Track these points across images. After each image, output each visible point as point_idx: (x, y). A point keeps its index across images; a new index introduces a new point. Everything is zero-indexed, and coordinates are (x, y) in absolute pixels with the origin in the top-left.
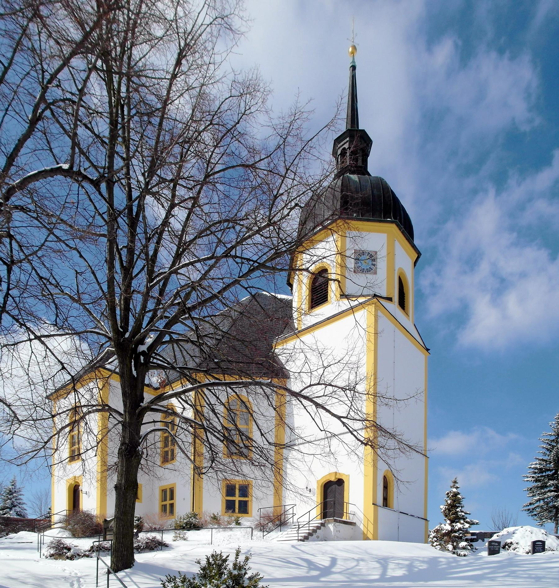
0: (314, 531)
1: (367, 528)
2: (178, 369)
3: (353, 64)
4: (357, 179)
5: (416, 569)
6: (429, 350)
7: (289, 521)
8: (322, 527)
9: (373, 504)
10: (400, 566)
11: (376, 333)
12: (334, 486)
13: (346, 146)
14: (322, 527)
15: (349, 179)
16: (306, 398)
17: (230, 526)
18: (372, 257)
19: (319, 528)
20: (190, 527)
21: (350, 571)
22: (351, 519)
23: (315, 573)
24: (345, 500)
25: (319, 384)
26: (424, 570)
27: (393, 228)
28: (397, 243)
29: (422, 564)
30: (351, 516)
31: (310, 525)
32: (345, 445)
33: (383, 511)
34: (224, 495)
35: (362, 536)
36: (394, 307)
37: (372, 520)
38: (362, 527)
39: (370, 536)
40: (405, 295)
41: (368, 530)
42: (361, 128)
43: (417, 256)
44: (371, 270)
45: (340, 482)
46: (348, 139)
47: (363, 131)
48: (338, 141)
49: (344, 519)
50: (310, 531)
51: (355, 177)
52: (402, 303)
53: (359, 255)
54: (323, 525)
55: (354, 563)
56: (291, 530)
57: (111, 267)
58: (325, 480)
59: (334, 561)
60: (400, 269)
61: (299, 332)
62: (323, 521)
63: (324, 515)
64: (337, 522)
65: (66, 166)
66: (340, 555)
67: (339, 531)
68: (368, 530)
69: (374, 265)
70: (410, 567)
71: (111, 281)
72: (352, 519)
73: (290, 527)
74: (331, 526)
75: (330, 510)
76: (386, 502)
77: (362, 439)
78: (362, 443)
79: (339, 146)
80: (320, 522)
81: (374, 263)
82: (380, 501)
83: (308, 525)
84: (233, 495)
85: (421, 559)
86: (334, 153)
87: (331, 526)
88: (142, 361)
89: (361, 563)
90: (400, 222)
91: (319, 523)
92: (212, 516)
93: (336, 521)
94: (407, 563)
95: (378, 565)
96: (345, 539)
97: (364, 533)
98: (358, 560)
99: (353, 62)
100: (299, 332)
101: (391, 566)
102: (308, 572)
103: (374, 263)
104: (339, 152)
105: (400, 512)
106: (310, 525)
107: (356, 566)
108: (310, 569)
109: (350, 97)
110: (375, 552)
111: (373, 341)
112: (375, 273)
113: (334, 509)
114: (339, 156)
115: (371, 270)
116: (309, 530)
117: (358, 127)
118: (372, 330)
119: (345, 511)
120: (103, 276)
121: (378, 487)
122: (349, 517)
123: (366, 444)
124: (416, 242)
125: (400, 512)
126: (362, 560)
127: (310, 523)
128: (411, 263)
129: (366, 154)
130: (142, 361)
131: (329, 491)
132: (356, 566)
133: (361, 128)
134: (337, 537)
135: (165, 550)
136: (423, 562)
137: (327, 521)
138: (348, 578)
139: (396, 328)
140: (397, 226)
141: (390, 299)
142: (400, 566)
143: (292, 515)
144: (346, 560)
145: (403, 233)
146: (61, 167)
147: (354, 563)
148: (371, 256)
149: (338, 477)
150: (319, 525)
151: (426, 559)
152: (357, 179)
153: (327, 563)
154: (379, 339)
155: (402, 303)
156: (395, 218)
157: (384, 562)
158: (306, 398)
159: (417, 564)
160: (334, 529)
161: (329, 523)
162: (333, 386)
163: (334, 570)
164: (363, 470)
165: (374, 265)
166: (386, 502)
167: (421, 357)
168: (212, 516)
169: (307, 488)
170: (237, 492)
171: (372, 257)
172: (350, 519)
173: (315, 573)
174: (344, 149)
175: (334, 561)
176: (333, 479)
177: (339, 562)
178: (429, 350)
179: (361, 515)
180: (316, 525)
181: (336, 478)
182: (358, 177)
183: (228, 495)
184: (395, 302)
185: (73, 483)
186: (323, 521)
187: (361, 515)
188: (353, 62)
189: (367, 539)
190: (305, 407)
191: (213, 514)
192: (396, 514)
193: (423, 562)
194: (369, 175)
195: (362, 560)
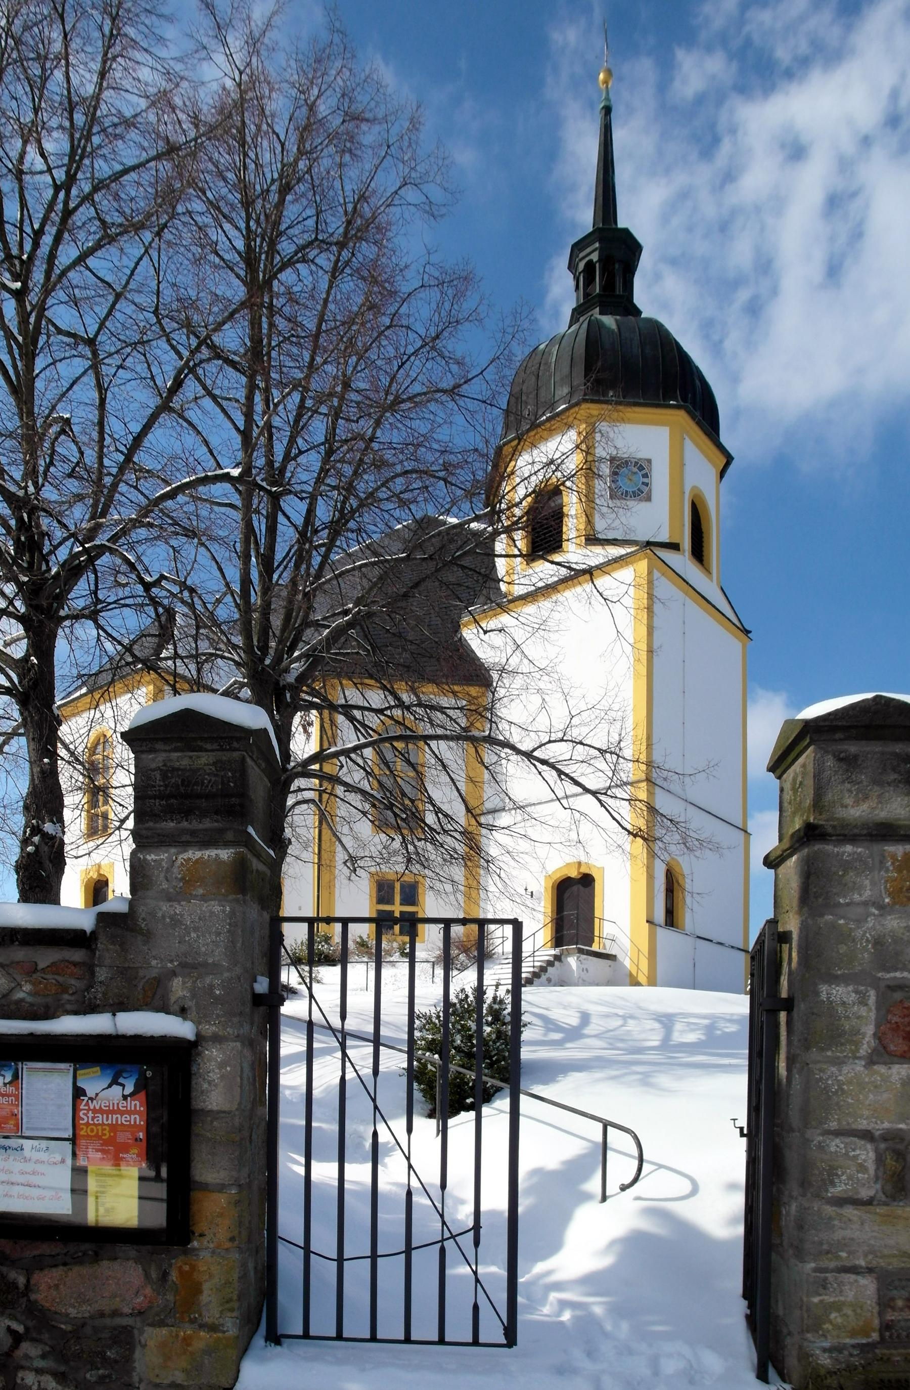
0: (543, 969)
1: (637, 966)
2: (340, 710)
3: (608, 104)
4: (614, 326)
5: (719, 1032)
6: (749, 632)
7: (496, 950)
8: (556, 963)
9: (647, 921)
10: (693, 1027)
11: (650, 651)
12: (575, 888)
13: (595, 257)
14: (556, 963)
15: (600, 325)
16: (544, 762)
17: (391, 959)
18: (642, 467)
19: (550, 964)
20: (319, 959)
21: (612, 1033)
22: (608, 947)
23: (557, 1036)
24: (597, 914)
25: (562, 740)
26: (733, 1033)
27: (681, 417)
28: (688, 443)
29: (728, 1025)
30: (608, 943)
31: (536, 959)
32: (601, 831)
33: (665, 935)
34: (375, 900)
35: (628, 980)
36: (682, 561)
37: (645, 949)
38: (627, 963)
39: (642, 979)
40: (704, 535)
41: (638, 968)
42: (621, 224)
43: (725, 461)
44: (643, 494)
45: (587, 881)
46: (597, 245)
47: (626, 231)
48: (578, 247)
49: (595, 947)
50: (536, 970)
51: (609, 321)
52: (699, 552)
53: (619, 465)
54: (558, 958)
55: (619, 1022)
56: (500, 966)
57: (246, 558)
58: (559, 876)
59: (585, 1018)
60: (694, 488)
61: (510, 602)
62: (557, 951)
63: (558, 940)
64: (583, 954)
65: (236, 472)
66: (592, 1008)
67: (587, 970)
68: (638, 968)
69: (647, 485)
70: (710, 1029)
71: (246, 581)
72: (610, 949)
73: (498, 962)
74: (572, 961)
75: (567, 933)
76: (671, 919)
77: (629, 827)
78: (629, 833)
79: (581, 255)
80: (553, 952)
81: (646, 480)
82: (660, 915)
83: (531, 959)
84: (390, 901)
85: (728, 1017)
86: (572, 266)
87: (572, 961)
88: (289, 700)
89: (631, 1022)
90: (694, 404)
91: (550, 955)
92: (358, 940)
93: (581, 951)
94: (706, 1022)
95: (657, 1025)
96: (598, 985)
97: (631, 975)
98: (625, 1018)
99: (607, 99)
100: (510, 602)
101: (678, 1026)
102: (545, 1035)
103: (646, 480)
104: (581, 266)
105: (698, 937)
106: (536, 959)
107: (622, 1026)
108: (548, 1030)
109: (602, 164)
110: (654, 1008)
111: (645, 662)
112: (649, 499)
113: (577, 930)
114: (580, 273)
115: (643, 494)
116: (534, 967)
117: (616, 222)
118: (644, 647)
119: (596, 933)
120: (233, 573)
121: (656, 901)
122: (604, 944)
123: (635, 836)
124: (724, 439)
125: (698, 937)
126: (632, 1017)
127: (536, 954)
128: (712, 473)
129: (630, 269)
130: (289, 700)
131: (566, 895)
132: (622, 1026)
133: (621, 224)
134: (584, 981)
135: (291, 999)
136: (731, 1021)
137: (565, 952)
138: (610, 1044)
139: (687, 598)
140: (689, 412)
141: (674, 546)
142: (693, 1027)
143: (501, 940)
144: (607, 1016)
145: (698, 423)
146: (228, 473)
147: (619, 1022)
148: (641, 468)
149: (584, 870)
150: (552, 959)
151: (735, 1017)
152: (614, 326)
153: (574, 1021)
154: (655, 659)
155: (699, 552)
156: (685, 400)
157: (667, 1021)
158: (544, 762)
159: (721, 1024)
160: (578, 967)
161: (569, 953)
162: (584, 745)
163: (586, 1031)
164: (629, 872)
165: (647, 485)
166: (671, 919)
167: (733, 644)
168: (358, 940)
169: (526, 890)
170: (397, 898)
171: (642, 467)
172: (605, 949)
173: (557, 1036)
174: (591, 261)
175: (585, 1018)
176: (574, 874)
177: (594, 1020)
178: (749, 632)
179: (625, 942)
180: (547, 958)
181: (579, 873)
182: (616, 321)
183: (380, 901)
184: (684, 551)
185: (95, 876)
186: (557, 951)
187: (625, 942)
188: (607, 99)
189: (637, 984)
190: (540, 773)
191: (361, 937)
192: (690, 941)
193: (731, 1021)
194: (638, 312)
195: (632, 1017)
